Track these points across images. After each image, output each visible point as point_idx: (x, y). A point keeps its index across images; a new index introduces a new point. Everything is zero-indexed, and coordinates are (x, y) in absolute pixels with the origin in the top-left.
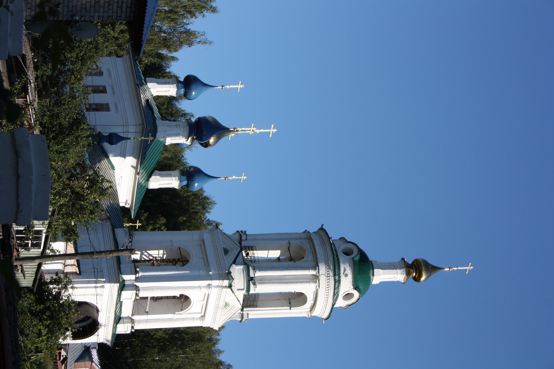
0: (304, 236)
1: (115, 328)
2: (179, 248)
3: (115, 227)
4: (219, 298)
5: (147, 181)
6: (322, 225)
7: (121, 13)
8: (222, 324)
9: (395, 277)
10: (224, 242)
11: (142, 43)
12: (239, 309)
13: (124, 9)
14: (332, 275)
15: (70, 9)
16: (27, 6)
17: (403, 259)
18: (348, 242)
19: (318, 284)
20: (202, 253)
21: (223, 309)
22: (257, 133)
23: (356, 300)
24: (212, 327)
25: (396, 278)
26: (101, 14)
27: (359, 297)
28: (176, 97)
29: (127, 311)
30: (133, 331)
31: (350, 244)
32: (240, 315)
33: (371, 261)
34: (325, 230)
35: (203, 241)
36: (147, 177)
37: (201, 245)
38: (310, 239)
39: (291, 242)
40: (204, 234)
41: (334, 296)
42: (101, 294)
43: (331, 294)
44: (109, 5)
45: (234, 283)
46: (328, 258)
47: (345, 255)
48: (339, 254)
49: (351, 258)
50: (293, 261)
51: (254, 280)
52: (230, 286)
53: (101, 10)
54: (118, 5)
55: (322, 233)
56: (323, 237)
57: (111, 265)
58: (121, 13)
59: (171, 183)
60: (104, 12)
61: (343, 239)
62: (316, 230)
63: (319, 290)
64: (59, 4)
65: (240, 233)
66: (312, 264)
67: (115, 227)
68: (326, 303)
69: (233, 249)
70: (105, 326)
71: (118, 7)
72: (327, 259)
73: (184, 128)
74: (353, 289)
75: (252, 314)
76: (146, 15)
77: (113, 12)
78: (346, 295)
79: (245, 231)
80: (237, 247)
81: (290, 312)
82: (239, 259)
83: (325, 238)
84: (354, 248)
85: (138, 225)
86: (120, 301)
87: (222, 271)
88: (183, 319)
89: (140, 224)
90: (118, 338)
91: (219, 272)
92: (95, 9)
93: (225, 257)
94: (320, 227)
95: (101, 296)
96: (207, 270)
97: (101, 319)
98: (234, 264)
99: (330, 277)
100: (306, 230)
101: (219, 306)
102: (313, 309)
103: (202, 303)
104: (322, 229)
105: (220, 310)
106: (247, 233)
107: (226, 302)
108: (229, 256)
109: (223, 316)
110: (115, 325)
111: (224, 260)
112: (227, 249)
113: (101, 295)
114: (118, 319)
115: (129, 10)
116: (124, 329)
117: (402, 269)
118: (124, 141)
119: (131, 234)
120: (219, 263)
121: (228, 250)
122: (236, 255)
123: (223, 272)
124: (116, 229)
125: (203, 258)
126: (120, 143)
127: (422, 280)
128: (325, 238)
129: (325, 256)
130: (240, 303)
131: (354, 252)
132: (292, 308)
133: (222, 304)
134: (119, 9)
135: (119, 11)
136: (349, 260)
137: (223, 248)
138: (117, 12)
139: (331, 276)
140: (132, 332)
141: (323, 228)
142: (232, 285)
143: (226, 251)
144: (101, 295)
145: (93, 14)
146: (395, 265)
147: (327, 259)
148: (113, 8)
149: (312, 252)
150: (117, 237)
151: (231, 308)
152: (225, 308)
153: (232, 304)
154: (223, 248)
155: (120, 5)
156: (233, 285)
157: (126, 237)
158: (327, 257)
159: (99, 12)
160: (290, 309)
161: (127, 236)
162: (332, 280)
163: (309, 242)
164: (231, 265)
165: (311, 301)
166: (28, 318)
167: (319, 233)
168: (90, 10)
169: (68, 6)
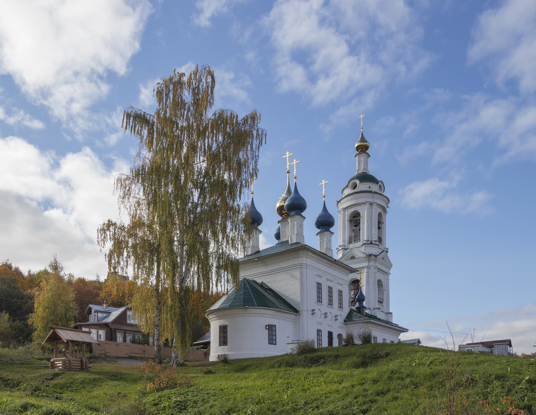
52: (376, 256)
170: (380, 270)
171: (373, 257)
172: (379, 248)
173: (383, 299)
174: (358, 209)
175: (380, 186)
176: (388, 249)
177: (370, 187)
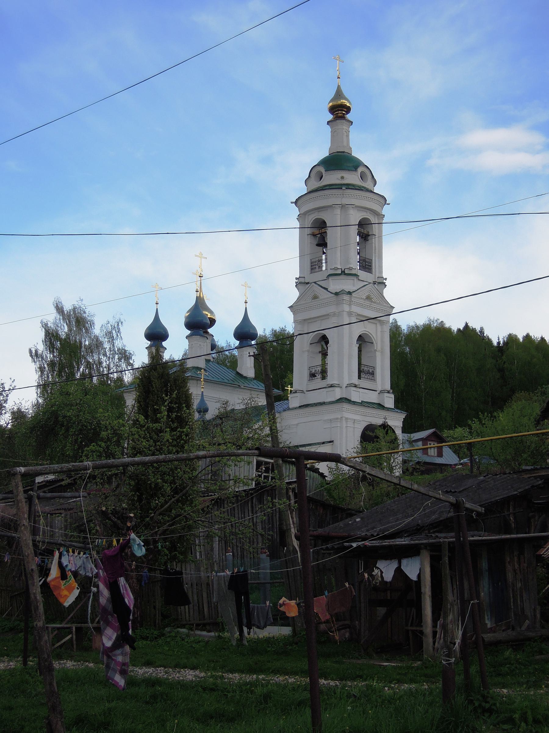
2: (311, 344)
4: (361, 305)
5: (247, 379)
6: (292, 203)
10: (306, 300)
14: (342, 192)
18: (309, 176)
19: (350, 206)
20: (316, 321)
23: (368, 169)
25: (346, 130)
29: (373, 397)
31: (311, 174)
37: (309, 323)
52: (350, 293)
79: (296, 279)
80: (311, 286)
82: (323, 284)
84: (315, 170)
86: (361, 403)
88: (382, 341)
89: (289, 386)
90: (400, 404)
93: (321, 297)
97: (379, 421)
99: (344, 193)
100: (297, 218)
104: (296, 203)
107: (366, 298)
111: (324, 299)
113: (354, 421)
114: (380, 406)
116: (389, 401)
118: (205, 399)
122: (319, 287)
125: (321, 320)
126: (207, 402)
130: (367, 284)
133: (367, 303)
140: (393, 393)
143: (315, 297)
144: (354, 421)
151: (372, 293)
162: (347, 192)
164: (329, 292)
166: (31, 686)
171: (346, 297)
174: (324, 216)
175: (363, 176)
176: (386, 279)
177: (342, 178)
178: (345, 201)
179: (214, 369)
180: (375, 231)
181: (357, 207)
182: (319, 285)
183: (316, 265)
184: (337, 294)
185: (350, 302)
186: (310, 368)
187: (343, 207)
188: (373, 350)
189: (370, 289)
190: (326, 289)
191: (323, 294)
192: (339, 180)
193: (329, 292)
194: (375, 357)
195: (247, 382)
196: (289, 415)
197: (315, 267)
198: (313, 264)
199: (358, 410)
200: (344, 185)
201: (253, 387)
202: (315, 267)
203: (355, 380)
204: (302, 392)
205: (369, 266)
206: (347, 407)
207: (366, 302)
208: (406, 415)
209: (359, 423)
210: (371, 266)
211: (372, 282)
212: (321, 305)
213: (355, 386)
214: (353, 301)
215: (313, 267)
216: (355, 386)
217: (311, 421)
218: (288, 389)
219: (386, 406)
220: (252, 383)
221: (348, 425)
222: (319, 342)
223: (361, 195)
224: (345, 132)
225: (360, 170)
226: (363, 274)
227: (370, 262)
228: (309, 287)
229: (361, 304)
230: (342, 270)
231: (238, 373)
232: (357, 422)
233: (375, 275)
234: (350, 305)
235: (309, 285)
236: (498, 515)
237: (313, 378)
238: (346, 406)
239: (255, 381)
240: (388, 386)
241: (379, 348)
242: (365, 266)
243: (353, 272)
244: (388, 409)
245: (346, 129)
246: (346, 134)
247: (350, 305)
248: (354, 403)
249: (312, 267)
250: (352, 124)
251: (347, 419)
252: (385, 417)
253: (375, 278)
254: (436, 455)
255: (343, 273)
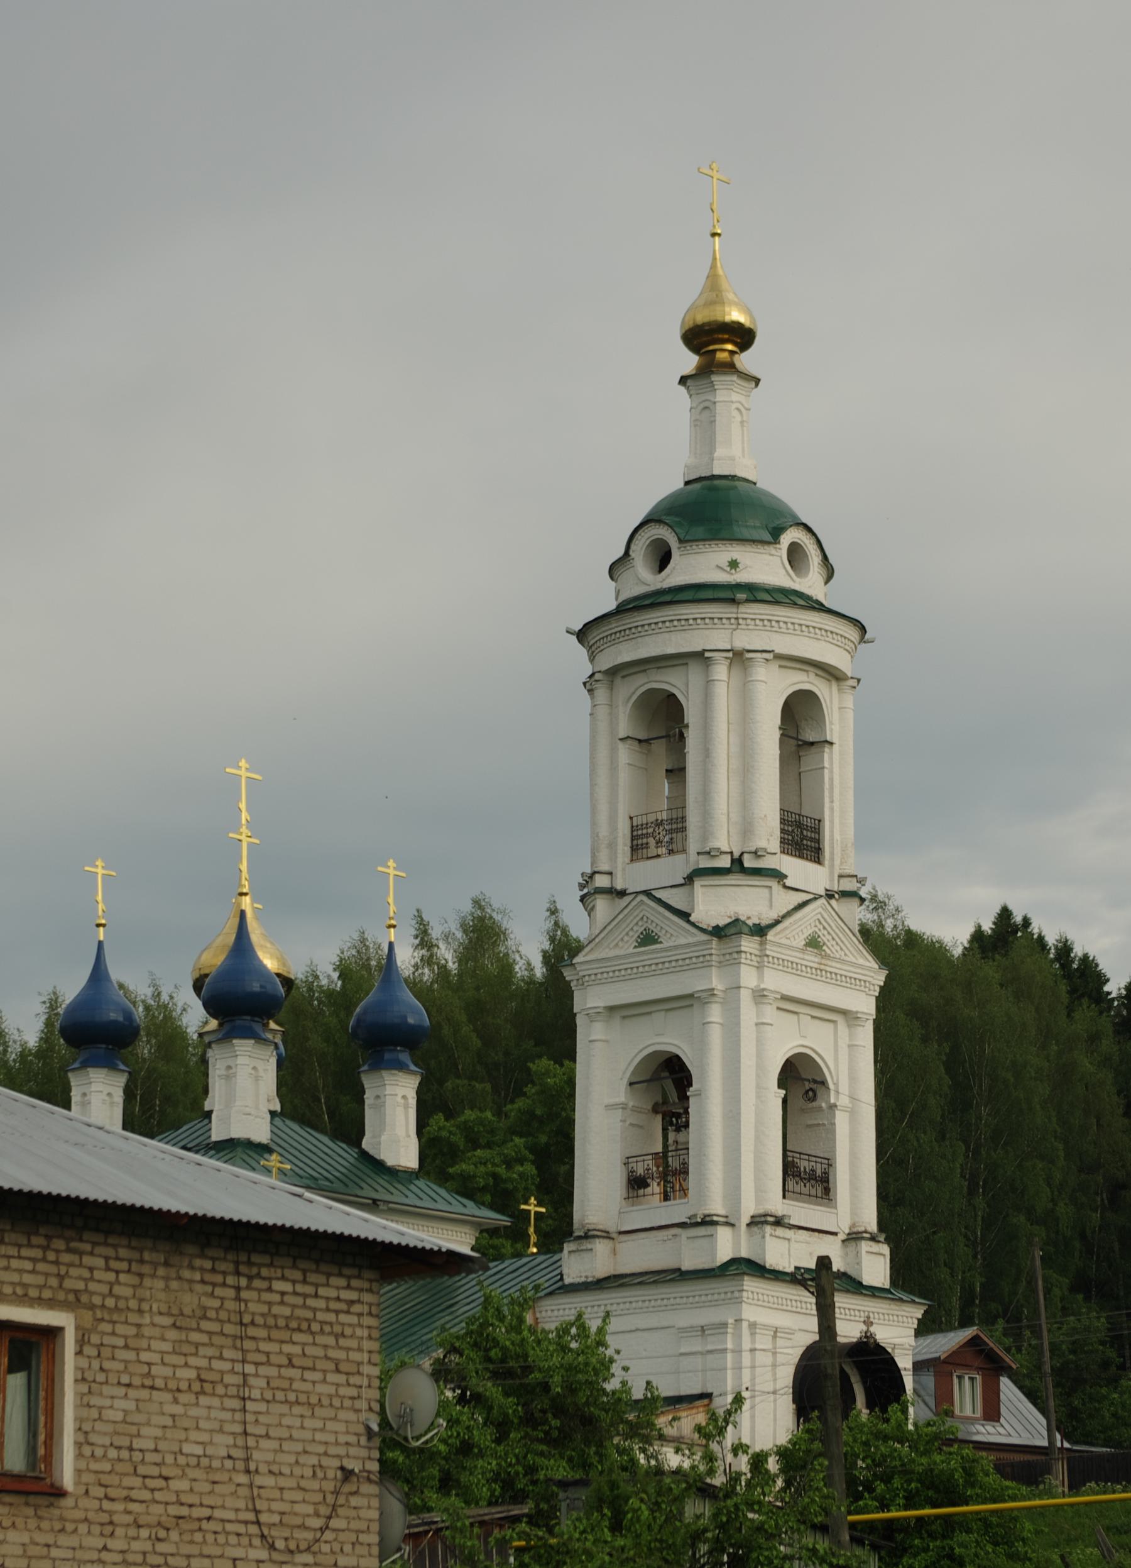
0: (601, 693)
1: (874, 1292)
3: (560, 1284)
4: (794, 969)
7: (363, 1303)
8: (870, 958)
9: (738, 409)
10: (617, 945)
11: (444, 1250)
12: (826, 903)
13: (352, 1295)
14: (735, 610)
15: (352, 1439)
16: (347, 1555)
17: (683, 380)
18: (627, 553)
19: (758, 655)
21: (827, 957)
22: (249, 819)
23: (809, 535)
24: (878, 989)
26: (366, 1356)
27: (801, 528)
28: (130, 1073)
30: (882, 1238)
31: (633, 547)
32: (843, 900)
33: (687, 483)
34: (585, 625)
35: (612, 1009)
36: (385, 1174)
38: (614, 672)
39: (622, 735)
40: (588, 1006)
41: (796, 604)
42: (772, 1333)
43: (789, 615)
44: (343, 1335)
45: (749, 918)
46: (679, 620)
47: (669, 566)
48: (666, 585)
49: (679, 548)
50: (684, 731)
51: (742, 854)
52: (760, 931)
53: (355, 1356)
54: (342, 1311)
55: (594, 636)
56: (610, 632)
57: (685, 1300)
58: (363, 1303)
59: (404, 1097)
60: (360, 1349)
61: (614, 570)
62: (582, 652)
63: (776, 651)
64: (342, 1468)
65: (586, 891)
66: (694, 674)
67: (560, 1284)
68: (804, 628)
69: (642, 918)
70: (868, 1323)
71: (348, 1312)
72: (683, 622)
73: (238, 1053)
74: (778, 546)
75: (842, 863)
76: (379, 1239)
77: (360, 1326)
78: (792, 567)
80: (634, 903)
81: (840, 746)
82: (675, 898)
83: (613, 625)
84: (647, 536)
85: (535, 1206)
86: (792, 1275)
87: (711, 955)
88: (853, 1079)
91: (714, 963)
92: (353, 1374)
94: (574, 637)
95: (778, 1334)
96: (707, 1003)
98: (689, 915)
100: (585, 684)
101: (816, 965)
102: (832, 670)
103: (806, 1019)
104: (582, 635)
105: (830, 963)
106: (589, 871)
107: (806, 945)
108: (664, 932)
109: (845, 955)
110: (864, 1292)
112: (639, 937)
113: (776, 1332)
115: (355, 1283)
117: (716, 387)
119: (582, 1234)
120: (687, 961)
121: (642, 933)
122: (662, 910)
123: (713, 951)
124: (567, 1280)
127: (746, 319)
128: (613, 625)
129: (672, 629)
131: (660, 537)
132: (828, 739)
133: (811, 958)
134: (352, 1310)
135: (356, 1308)
136: (686, 552)
137: (635, 947)
138: (360, 1315)
139: (737, 613)
140: (887, 1241)
141: (580, 630)
142: (754, 925)
143: (648, 939)
144: (776, 1332)
145: (365, 1378)
146: (702, 406)
147: (683, 622)
148: (350, 1325)
149: (658, 668)
150: (594, 1277)
151: (824, 928)
152: (825, 948)
153: (813, 925)
154: (635, 947)
155: (344, 1306)
156: (757, 922)
157: (591, 1250)
158: (676, 623)
159: (359, 1364)
160: (831, 744)
161: (589, 1246)
162: (749, 611)
163: (623, 677)
164: (693, 924)
165: (808, 677)
167: (593, 644)
168: (355, 1386)
169: (347, 1444)
170: (791, 1003)
171: (748, 944)
172: (785, 887)
173: (830, 1163)
174: (671, 681)
177: (734, 564)
178: (743, 640)
179: (299, 1147)
180: (831, 730)
181: (779, 657)
182: (659, 901)
183: (647, 835)
184: (718, 932)
185: (758, 959)
186: (630, 1160)
187: (739, 657)
188: (824, 1105)
189: (819, 916)
190: (685, 916)
191: (674, 935)
192: (724, 570)
193: (693, 924)
194: (830, 1130)
195: (400, 1186)
196: (563, 1306)
197: (645, 841)
198: (640, 832)
199: (784, 1295)
200: (739, 587)
201: (419, 1203)
202: (645, 841)
203: (777, 1204)
204: (607, 1235)
205: (811, 839)
206: (753, 1289)
207: (806, 957)
208: (925, 1308)
209: (790, 1336)
210: (818, 841)
211: (823, 893)
212: (667, 965)
213: (779, 1222)
214: (768, 956)
215: (640, 842)
216: (779, 1222)
217: (637, 1330)
218: (529, 1211)
219: (867, 1281)
220: (412, 1187)
221: (758, 1346)
222: (654, 1079)
223: (793, 620)
224: (735, 413)
225: (790, 536)
226: (796, 869)
227: (817, 827)
228: (630, 907)
229: (792, 963)
230: (732, 856)
231: (365, 1157)
232: (782, 1335)
233: (832, 866)
234: (760, 968)
235: (627, 899)
236: (1047, 1368)
237: (641, 1192)
238: (751, 1286)
239: (421, 1183)
240: (870, 1219)
241: (843, 1101)
242: (802, 840)
243: (767, 863)
244: (874, 1292)
245: (740, 402)
246: (738, 418)
247: (760, 968)
248: (776, 1275)
249: (635, 842)
250: (757, 385)
251: (753, 1326)
252: (869, 1317)
253: (832, 880)
254: (979, 1414)
255: (738, 865)
